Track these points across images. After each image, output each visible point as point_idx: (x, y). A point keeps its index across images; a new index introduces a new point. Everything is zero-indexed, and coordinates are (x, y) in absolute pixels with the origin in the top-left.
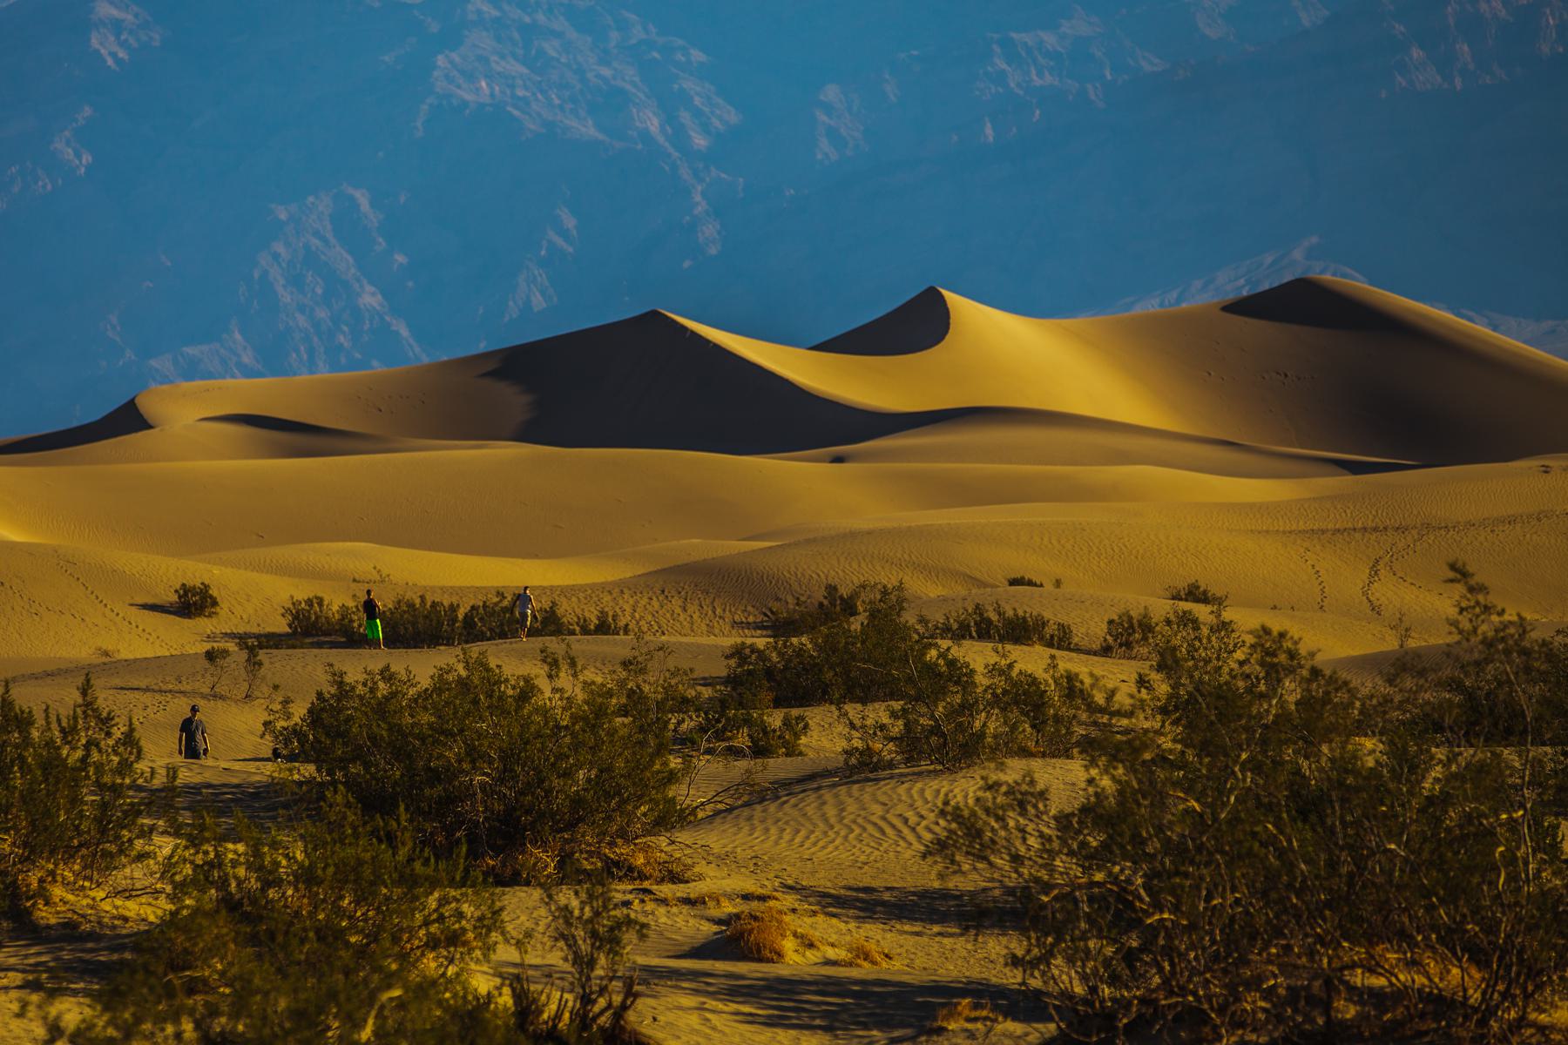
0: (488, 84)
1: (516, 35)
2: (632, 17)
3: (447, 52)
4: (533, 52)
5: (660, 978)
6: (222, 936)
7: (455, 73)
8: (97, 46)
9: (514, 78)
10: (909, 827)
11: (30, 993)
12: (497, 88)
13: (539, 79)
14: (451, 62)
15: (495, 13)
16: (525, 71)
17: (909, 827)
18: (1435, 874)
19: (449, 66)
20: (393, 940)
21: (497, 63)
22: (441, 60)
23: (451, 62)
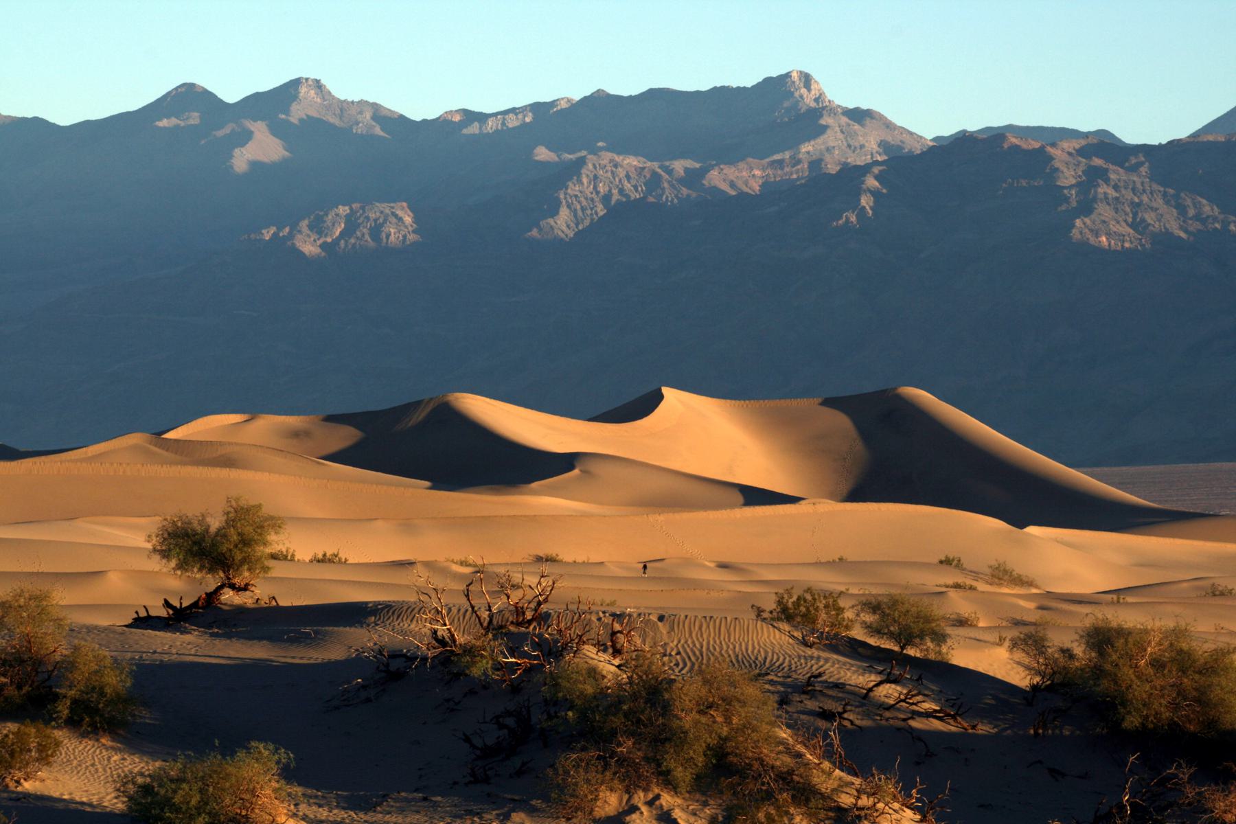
0: (1107, 239)
1: (1128, 209)
2: (1204, 201)
3: (1082, 217)
4: (1138, 220)
5: (920, 716)
6: (640, 765)
7: (1087, 230)
8: (865, 205)
9: (1124, 236)
10: (482, 723)
11: (145, 782)
12: (1113, 242)
13: (1140, 237)
14: (1084, 224)
15: (1115, 194)
16: (1132, 231)
17: (482, 723)
18: (1192, 727)
19: (1083, 226)
20: (786, 704)
21: (1113, 225)
22: (1078, 222)
23: (1084, 224)
